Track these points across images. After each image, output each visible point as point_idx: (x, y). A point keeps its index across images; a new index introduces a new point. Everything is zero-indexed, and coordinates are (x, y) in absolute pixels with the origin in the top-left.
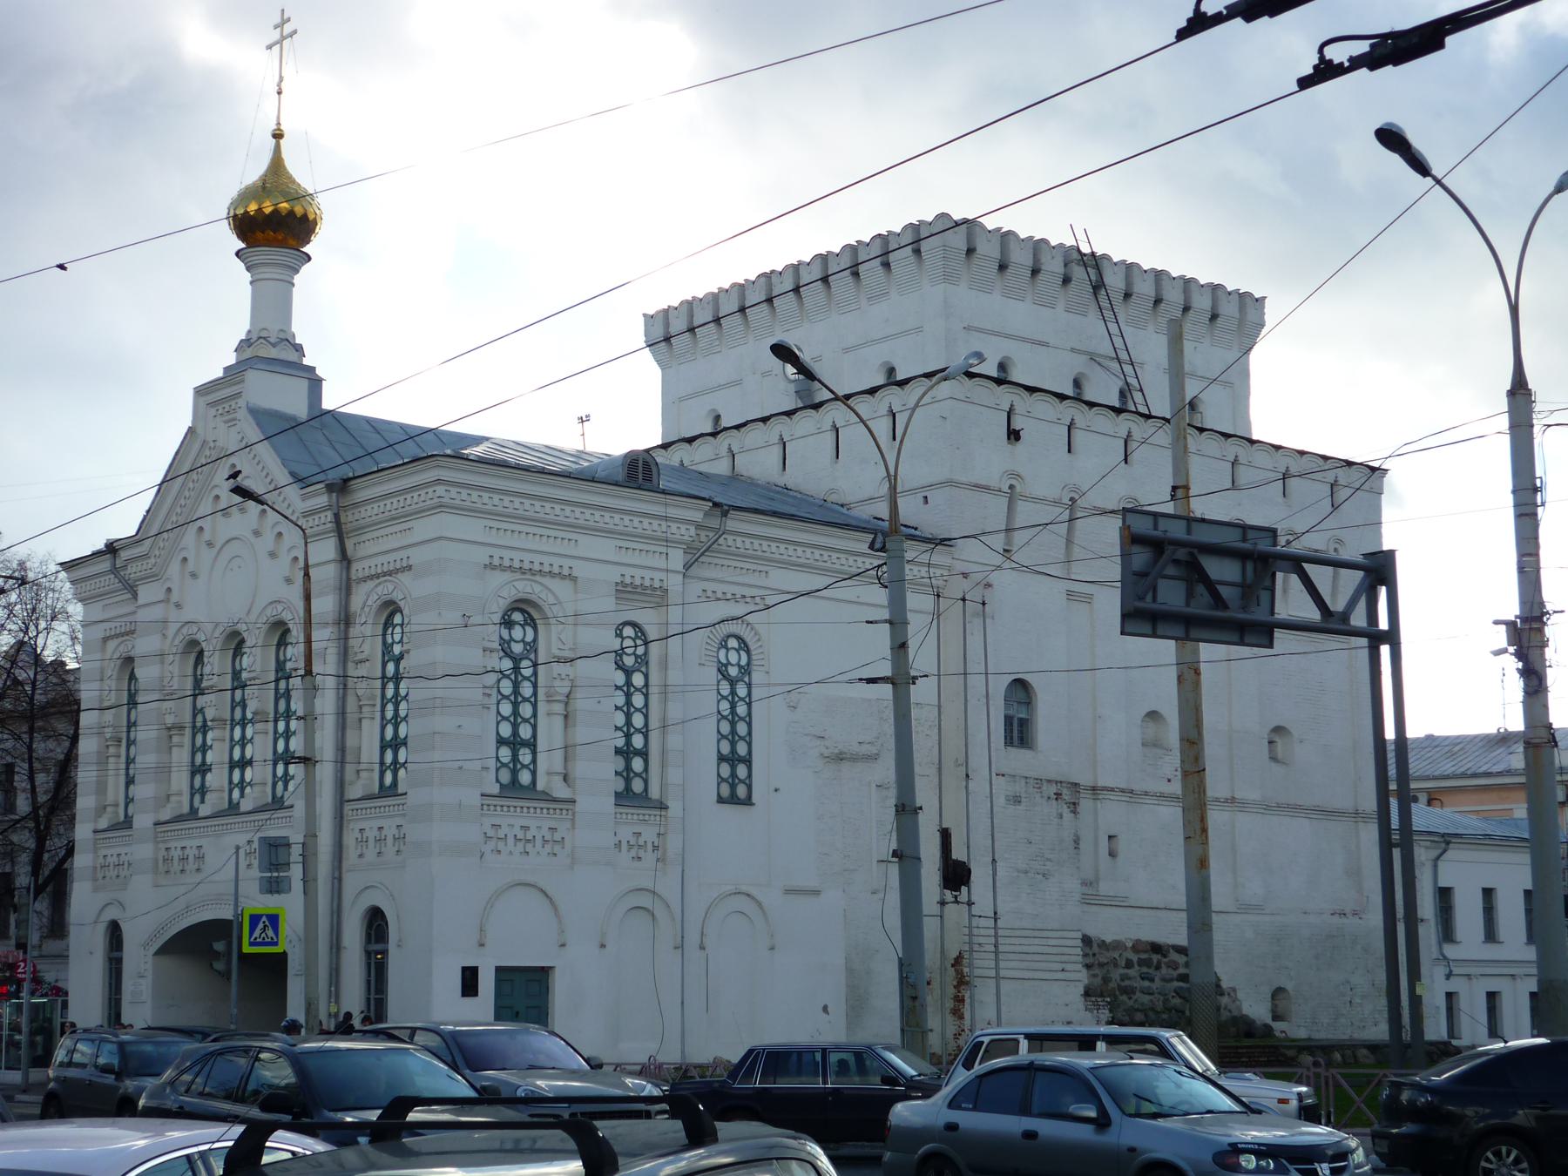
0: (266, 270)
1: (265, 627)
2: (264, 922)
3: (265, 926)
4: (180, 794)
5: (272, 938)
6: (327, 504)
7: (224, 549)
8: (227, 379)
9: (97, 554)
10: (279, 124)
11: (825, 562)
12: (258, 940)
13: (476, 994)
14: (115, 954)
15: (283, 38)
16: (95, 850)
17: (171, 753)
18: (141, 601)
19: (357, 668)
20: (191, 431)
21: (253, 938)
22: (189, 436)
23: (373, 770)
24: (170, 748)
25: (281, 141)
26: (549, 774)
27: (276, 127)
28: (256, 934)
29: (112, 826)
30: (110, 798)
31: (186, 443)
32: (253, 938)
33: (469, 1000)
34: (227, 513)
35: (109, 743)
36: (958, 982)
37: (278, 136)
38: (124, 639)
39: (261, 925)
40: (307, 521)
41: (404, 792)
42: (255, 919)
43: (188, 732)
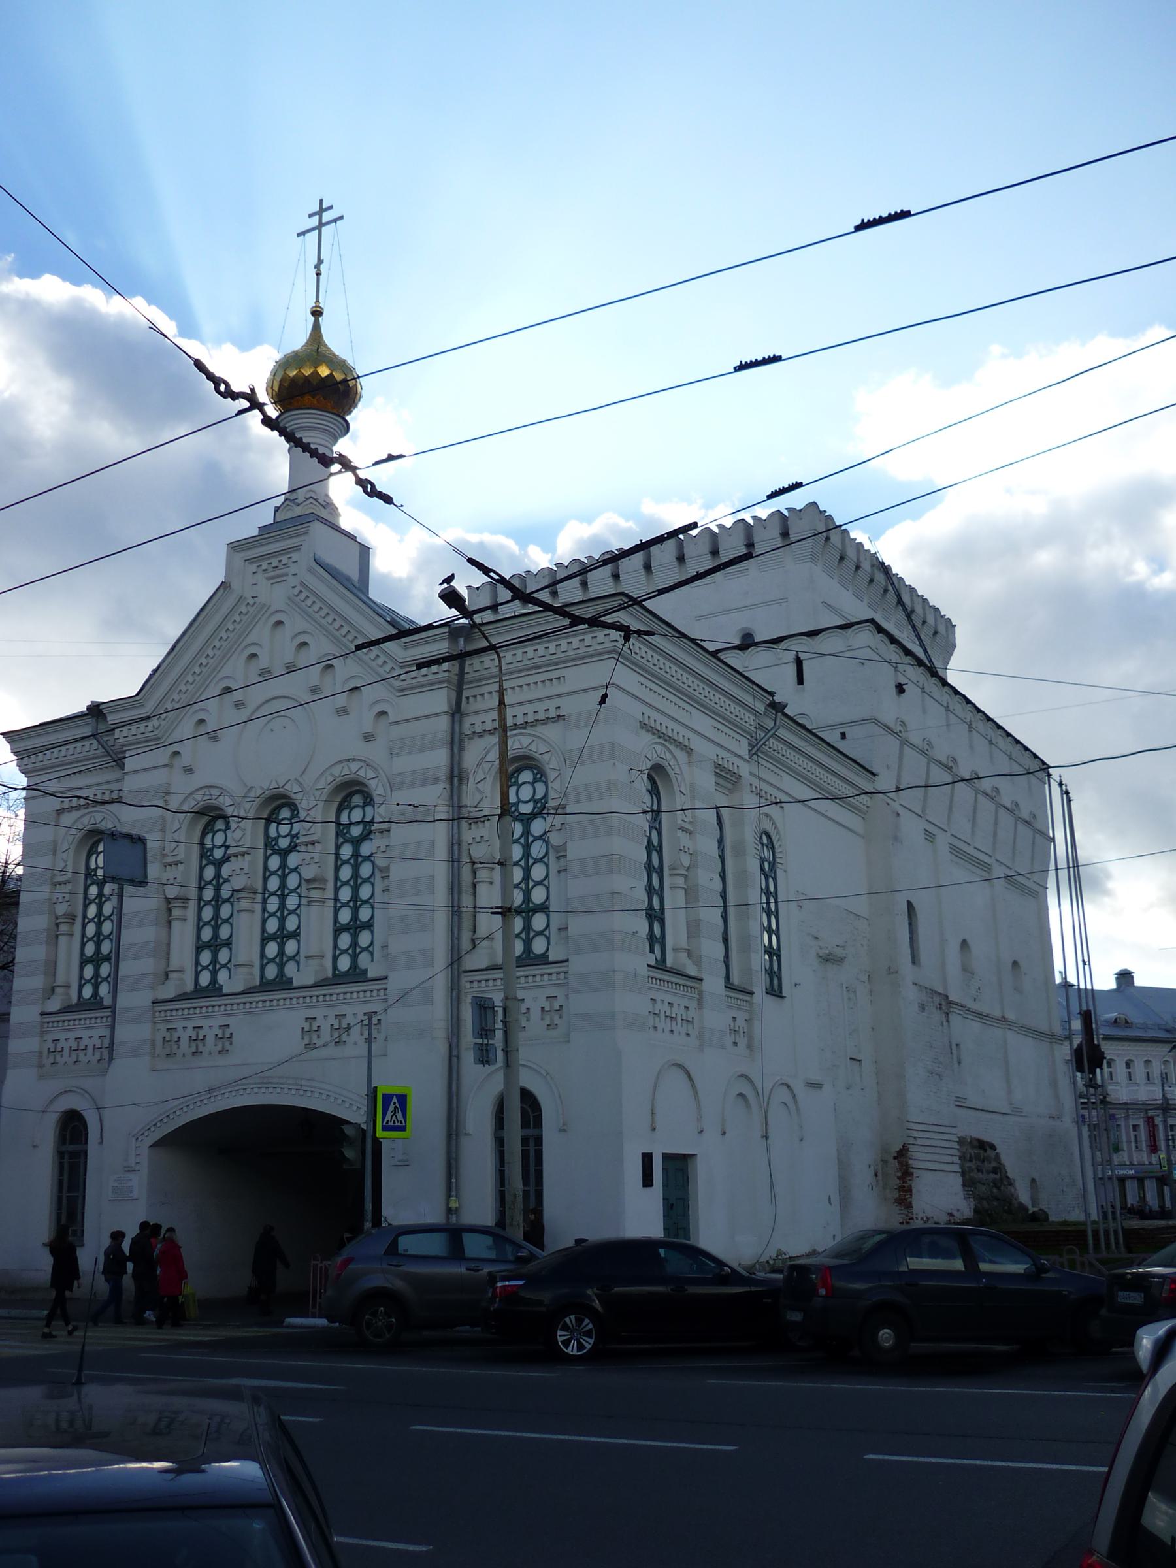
0: (312, 435)
1: (79, 835)
2: (395, 1103)
3: (396, 1108)
4: (181, 971)
5: (401, 1123)
6: (447, 650)
7: (281, 700)
8: (261, 537)
9: (81, 716)
10: (317, 301)
11: (27, 765)
12: (390, 1124)
13: (652, 1185)
14: (531, 1132)
15: (321, 224)
16: (42, 1034)
17: (57, 943)
18: (128, 768)
19: (470, 829)
20: (223, 585)
21: (385, 1122)
22: (221, 591)
23: (253, 966)
24: (57, 936)
25: (320, 319)
26: (675, 950)
27: (314, 305)
28: (388, 1117)
29: (65, 1008)
30: (61, 979)
31: (215, 599)
32: (385, 1122)
33: (647, 1190)
34: (287, 668)
35: (59, 921)
36: (903, 1174)
37: (317, 313)
38: (87, 811)
39: (392, 1107)
40: (52, 753)
41: (565, 958)
42: (387, 1098)
43: (192, 905)
